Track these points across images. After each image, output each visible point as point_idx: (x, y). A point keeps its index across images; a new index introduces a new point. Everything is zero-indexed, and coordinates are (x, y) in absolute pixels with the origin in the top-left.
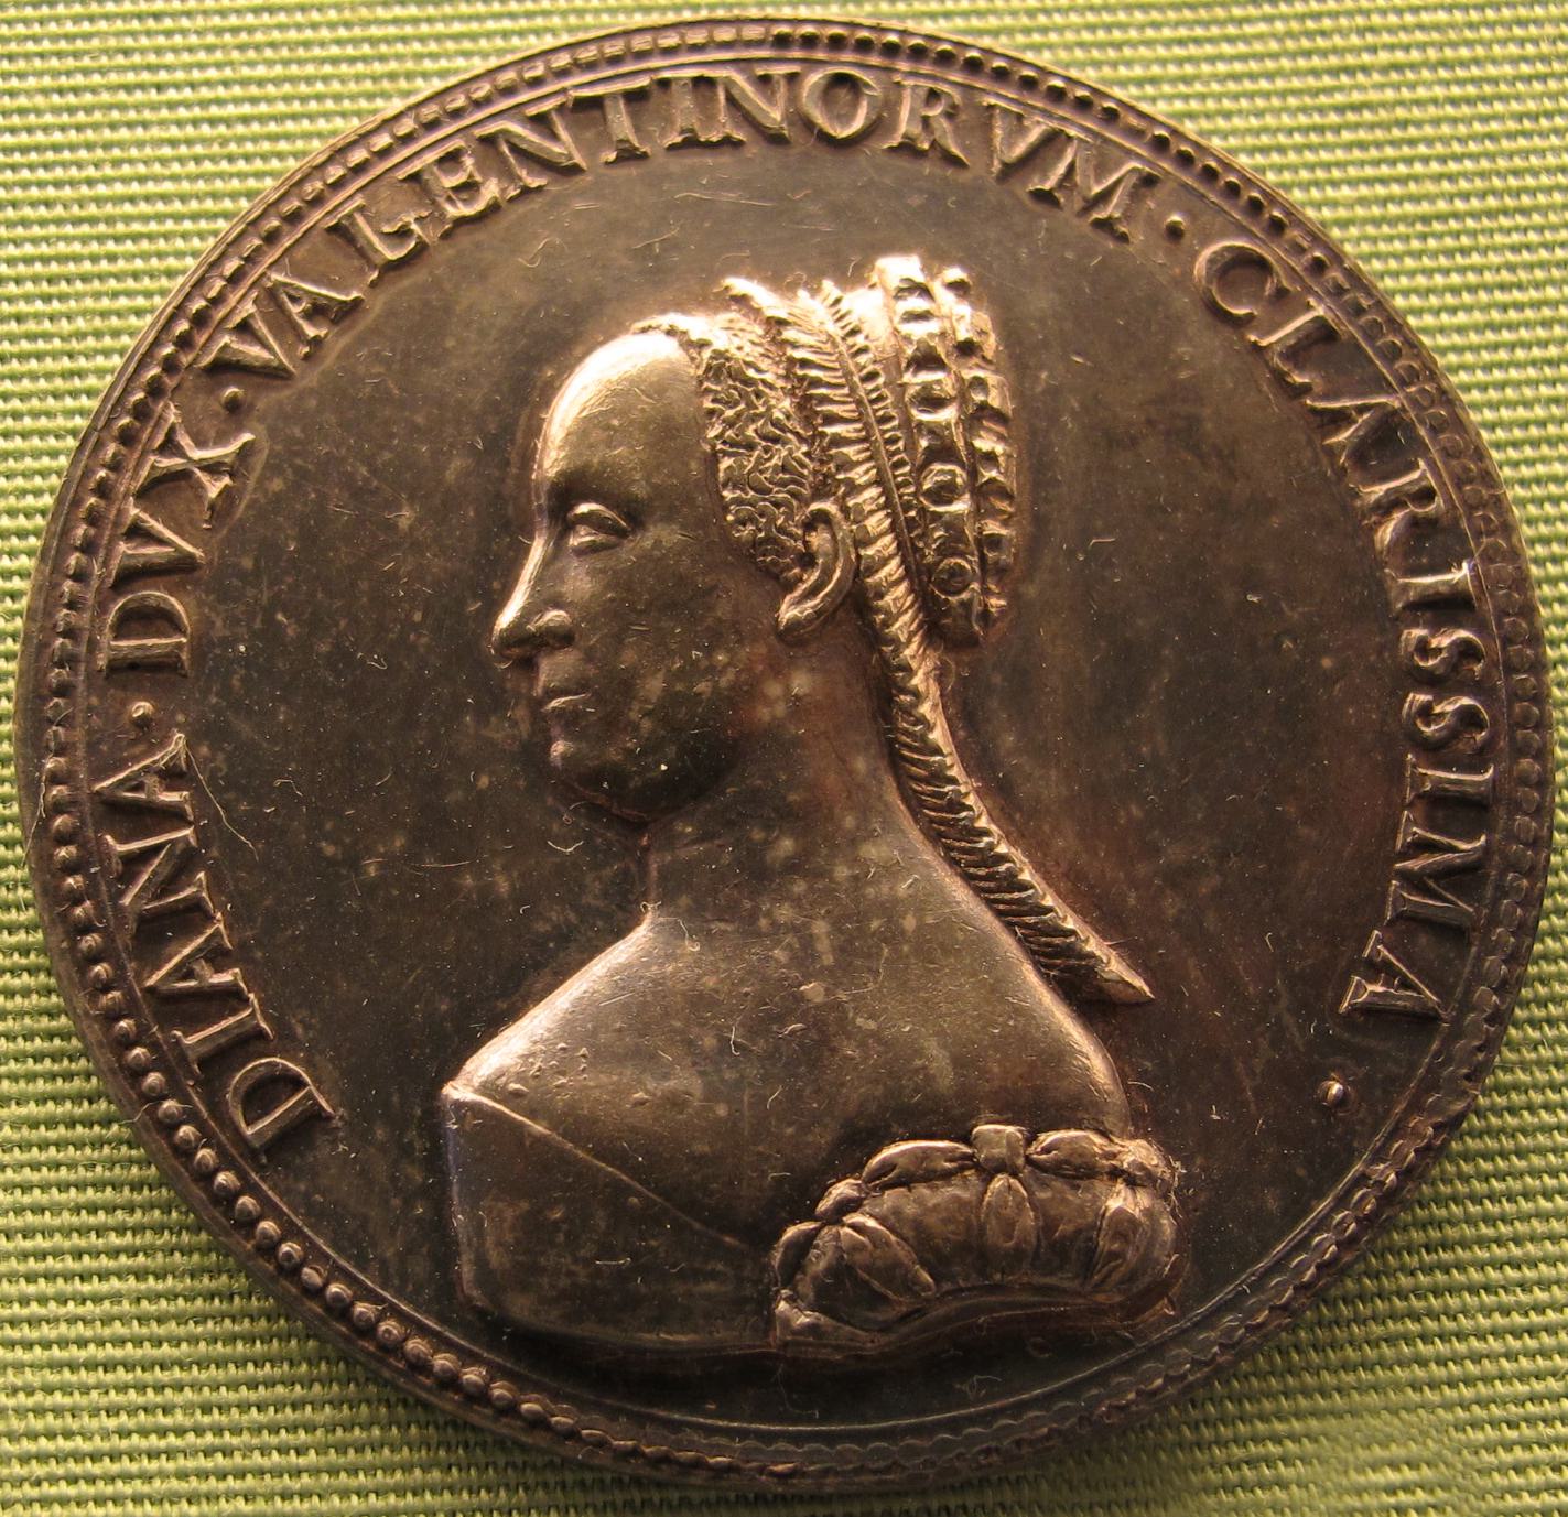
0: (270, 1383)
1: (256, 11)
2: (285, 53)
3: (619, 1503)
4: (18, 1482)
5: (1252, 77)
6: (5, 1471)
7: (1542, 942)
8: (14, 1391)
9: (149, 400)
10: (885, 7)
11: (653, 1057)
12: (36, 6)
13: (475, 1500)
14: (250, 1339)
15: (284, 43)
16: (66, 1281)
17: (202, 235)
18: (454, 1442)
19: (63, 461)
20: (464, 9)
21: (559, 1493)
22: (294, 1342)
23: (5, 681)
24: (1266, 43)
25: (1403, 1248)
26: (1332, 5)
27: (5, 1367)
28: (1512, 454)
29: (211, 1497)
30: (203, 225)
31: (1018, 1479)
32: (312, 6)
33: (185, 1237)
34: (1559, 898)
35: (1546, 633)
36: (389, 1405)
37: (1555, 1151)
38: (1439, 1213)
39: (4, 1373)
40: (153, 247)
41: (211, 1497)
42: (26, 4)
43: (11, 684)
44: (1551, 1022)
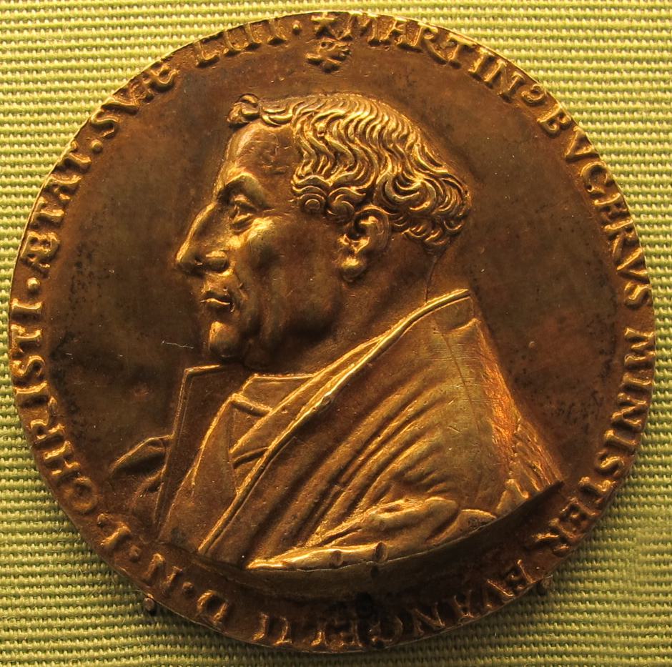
4: (8, 41)
6: (2, 549)
7: (653, 404)
8: (6, 206)
9: (65, 437)
10: (323, 3)
16: (53, 31)
18: (223, 654)
19: (12, 271)
21: (270, 658)
23: (3, 354)
26: (55, 3)
27: (2, 405)
28: (655, 260)
29: (109, 659)
31: (455, 637)
32: (100, 5)
34: (666, 372)
35: (656, 363)
36: (192, 636)
38: (541, 627)
39: (2, 219)
40: (82, 75)
41: (109, 659)
43: (8, 283)
44: (663, 412)
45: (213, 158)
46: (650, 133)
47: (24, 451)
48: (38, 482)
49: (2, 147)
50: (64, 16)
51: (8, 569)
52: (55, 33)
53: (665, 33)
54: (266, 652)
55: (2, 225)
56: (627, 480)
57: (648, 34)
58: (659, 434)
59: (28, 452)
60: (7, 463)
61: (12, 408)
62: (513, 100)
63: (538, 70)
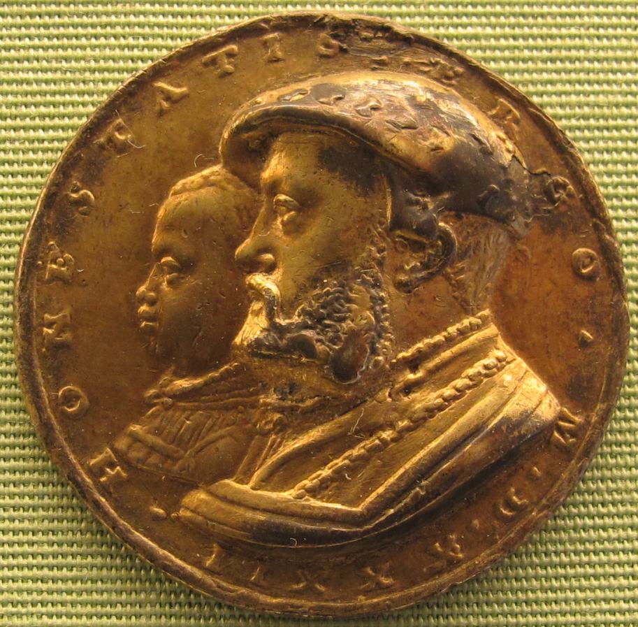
0: (42, 496)
1: (456, 5)
2: (437, 20)
3: (228, 616)
5: (93, 26)
11: (502, 563)
12: (153, 4)
13: (162, 610)
14: (52, 496)
15: (550, 14)
17: (115, 81)
20: (138, 7)
22: (133, 571)
24: (620, 18)
25: (580, 503)
28: (625, 224)
30: (116, 75)
33: (40, 463)
37: (631, 454)
42: (98, 3)
45: (93, 159)
46: (588, 28)
47: (14, 390)
48: (36, 451)
49: (3, 606)
50: (36, 613)
51: (7, 167)
52: (6, 488)
53: (630, 122)
54: (247, 615)
55: (2, 196)
56: (594, 460)
57: (602, 76)
58: (593, 154)
59: (18, 391)
60: (8, 417)
61: (10, 332)
62: (284, 148)
63: (428, 26)
